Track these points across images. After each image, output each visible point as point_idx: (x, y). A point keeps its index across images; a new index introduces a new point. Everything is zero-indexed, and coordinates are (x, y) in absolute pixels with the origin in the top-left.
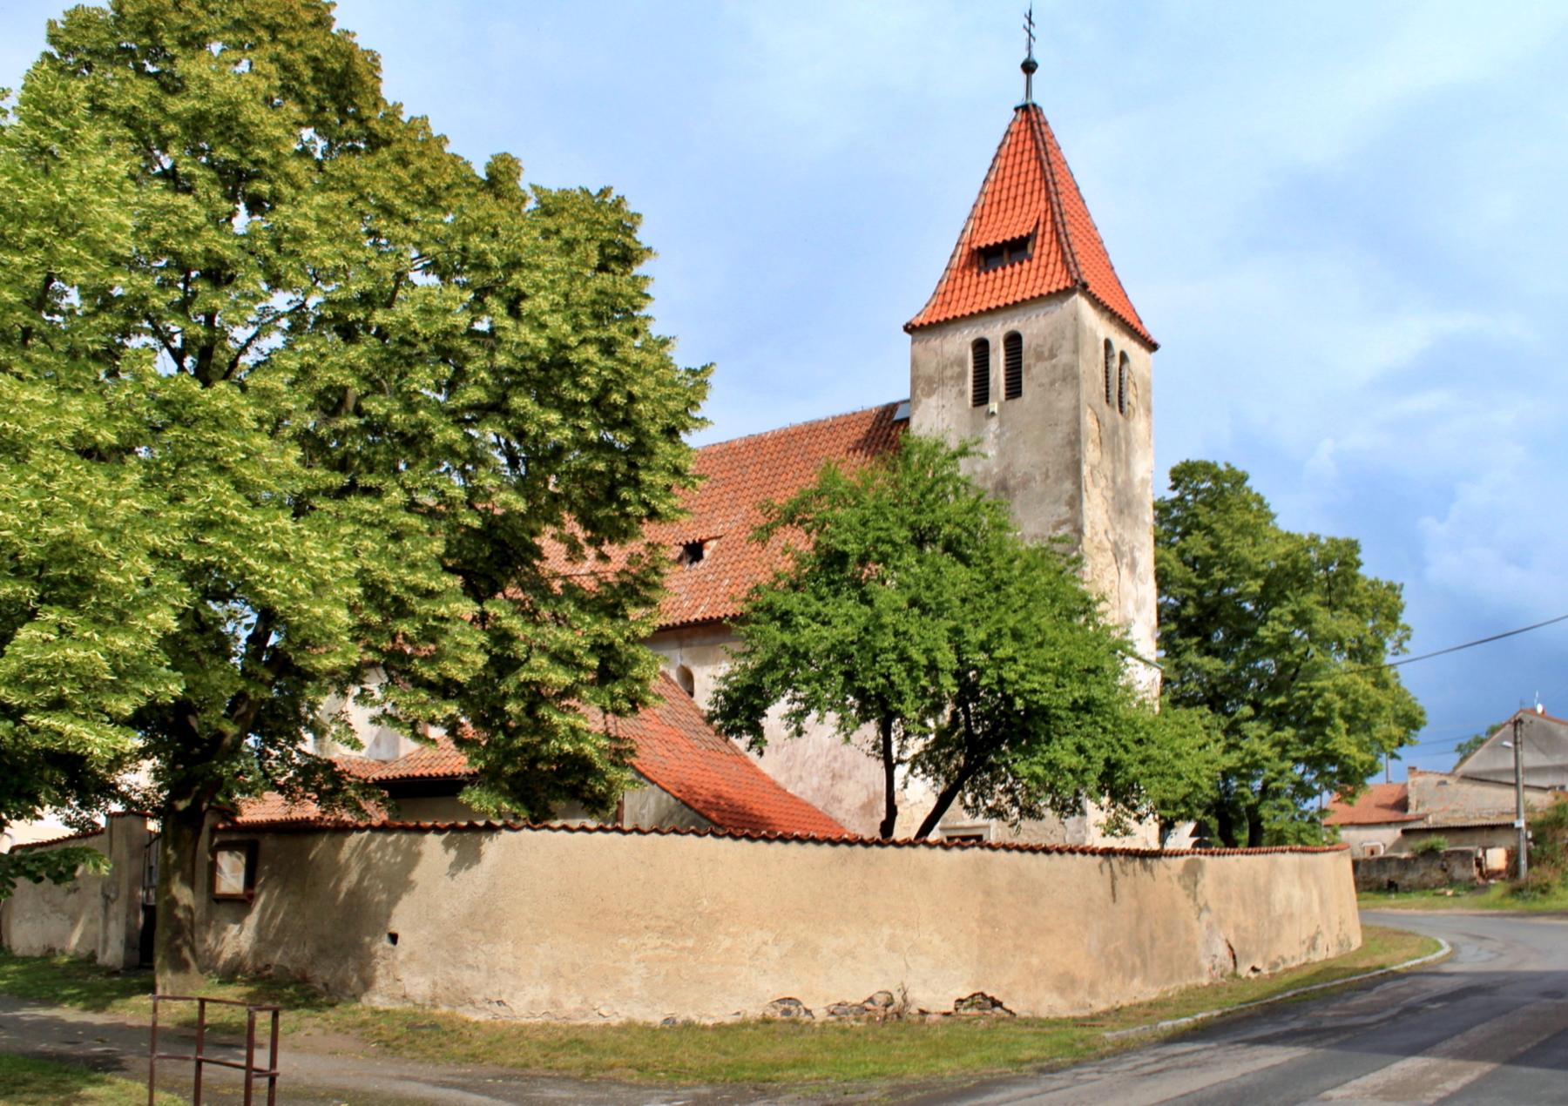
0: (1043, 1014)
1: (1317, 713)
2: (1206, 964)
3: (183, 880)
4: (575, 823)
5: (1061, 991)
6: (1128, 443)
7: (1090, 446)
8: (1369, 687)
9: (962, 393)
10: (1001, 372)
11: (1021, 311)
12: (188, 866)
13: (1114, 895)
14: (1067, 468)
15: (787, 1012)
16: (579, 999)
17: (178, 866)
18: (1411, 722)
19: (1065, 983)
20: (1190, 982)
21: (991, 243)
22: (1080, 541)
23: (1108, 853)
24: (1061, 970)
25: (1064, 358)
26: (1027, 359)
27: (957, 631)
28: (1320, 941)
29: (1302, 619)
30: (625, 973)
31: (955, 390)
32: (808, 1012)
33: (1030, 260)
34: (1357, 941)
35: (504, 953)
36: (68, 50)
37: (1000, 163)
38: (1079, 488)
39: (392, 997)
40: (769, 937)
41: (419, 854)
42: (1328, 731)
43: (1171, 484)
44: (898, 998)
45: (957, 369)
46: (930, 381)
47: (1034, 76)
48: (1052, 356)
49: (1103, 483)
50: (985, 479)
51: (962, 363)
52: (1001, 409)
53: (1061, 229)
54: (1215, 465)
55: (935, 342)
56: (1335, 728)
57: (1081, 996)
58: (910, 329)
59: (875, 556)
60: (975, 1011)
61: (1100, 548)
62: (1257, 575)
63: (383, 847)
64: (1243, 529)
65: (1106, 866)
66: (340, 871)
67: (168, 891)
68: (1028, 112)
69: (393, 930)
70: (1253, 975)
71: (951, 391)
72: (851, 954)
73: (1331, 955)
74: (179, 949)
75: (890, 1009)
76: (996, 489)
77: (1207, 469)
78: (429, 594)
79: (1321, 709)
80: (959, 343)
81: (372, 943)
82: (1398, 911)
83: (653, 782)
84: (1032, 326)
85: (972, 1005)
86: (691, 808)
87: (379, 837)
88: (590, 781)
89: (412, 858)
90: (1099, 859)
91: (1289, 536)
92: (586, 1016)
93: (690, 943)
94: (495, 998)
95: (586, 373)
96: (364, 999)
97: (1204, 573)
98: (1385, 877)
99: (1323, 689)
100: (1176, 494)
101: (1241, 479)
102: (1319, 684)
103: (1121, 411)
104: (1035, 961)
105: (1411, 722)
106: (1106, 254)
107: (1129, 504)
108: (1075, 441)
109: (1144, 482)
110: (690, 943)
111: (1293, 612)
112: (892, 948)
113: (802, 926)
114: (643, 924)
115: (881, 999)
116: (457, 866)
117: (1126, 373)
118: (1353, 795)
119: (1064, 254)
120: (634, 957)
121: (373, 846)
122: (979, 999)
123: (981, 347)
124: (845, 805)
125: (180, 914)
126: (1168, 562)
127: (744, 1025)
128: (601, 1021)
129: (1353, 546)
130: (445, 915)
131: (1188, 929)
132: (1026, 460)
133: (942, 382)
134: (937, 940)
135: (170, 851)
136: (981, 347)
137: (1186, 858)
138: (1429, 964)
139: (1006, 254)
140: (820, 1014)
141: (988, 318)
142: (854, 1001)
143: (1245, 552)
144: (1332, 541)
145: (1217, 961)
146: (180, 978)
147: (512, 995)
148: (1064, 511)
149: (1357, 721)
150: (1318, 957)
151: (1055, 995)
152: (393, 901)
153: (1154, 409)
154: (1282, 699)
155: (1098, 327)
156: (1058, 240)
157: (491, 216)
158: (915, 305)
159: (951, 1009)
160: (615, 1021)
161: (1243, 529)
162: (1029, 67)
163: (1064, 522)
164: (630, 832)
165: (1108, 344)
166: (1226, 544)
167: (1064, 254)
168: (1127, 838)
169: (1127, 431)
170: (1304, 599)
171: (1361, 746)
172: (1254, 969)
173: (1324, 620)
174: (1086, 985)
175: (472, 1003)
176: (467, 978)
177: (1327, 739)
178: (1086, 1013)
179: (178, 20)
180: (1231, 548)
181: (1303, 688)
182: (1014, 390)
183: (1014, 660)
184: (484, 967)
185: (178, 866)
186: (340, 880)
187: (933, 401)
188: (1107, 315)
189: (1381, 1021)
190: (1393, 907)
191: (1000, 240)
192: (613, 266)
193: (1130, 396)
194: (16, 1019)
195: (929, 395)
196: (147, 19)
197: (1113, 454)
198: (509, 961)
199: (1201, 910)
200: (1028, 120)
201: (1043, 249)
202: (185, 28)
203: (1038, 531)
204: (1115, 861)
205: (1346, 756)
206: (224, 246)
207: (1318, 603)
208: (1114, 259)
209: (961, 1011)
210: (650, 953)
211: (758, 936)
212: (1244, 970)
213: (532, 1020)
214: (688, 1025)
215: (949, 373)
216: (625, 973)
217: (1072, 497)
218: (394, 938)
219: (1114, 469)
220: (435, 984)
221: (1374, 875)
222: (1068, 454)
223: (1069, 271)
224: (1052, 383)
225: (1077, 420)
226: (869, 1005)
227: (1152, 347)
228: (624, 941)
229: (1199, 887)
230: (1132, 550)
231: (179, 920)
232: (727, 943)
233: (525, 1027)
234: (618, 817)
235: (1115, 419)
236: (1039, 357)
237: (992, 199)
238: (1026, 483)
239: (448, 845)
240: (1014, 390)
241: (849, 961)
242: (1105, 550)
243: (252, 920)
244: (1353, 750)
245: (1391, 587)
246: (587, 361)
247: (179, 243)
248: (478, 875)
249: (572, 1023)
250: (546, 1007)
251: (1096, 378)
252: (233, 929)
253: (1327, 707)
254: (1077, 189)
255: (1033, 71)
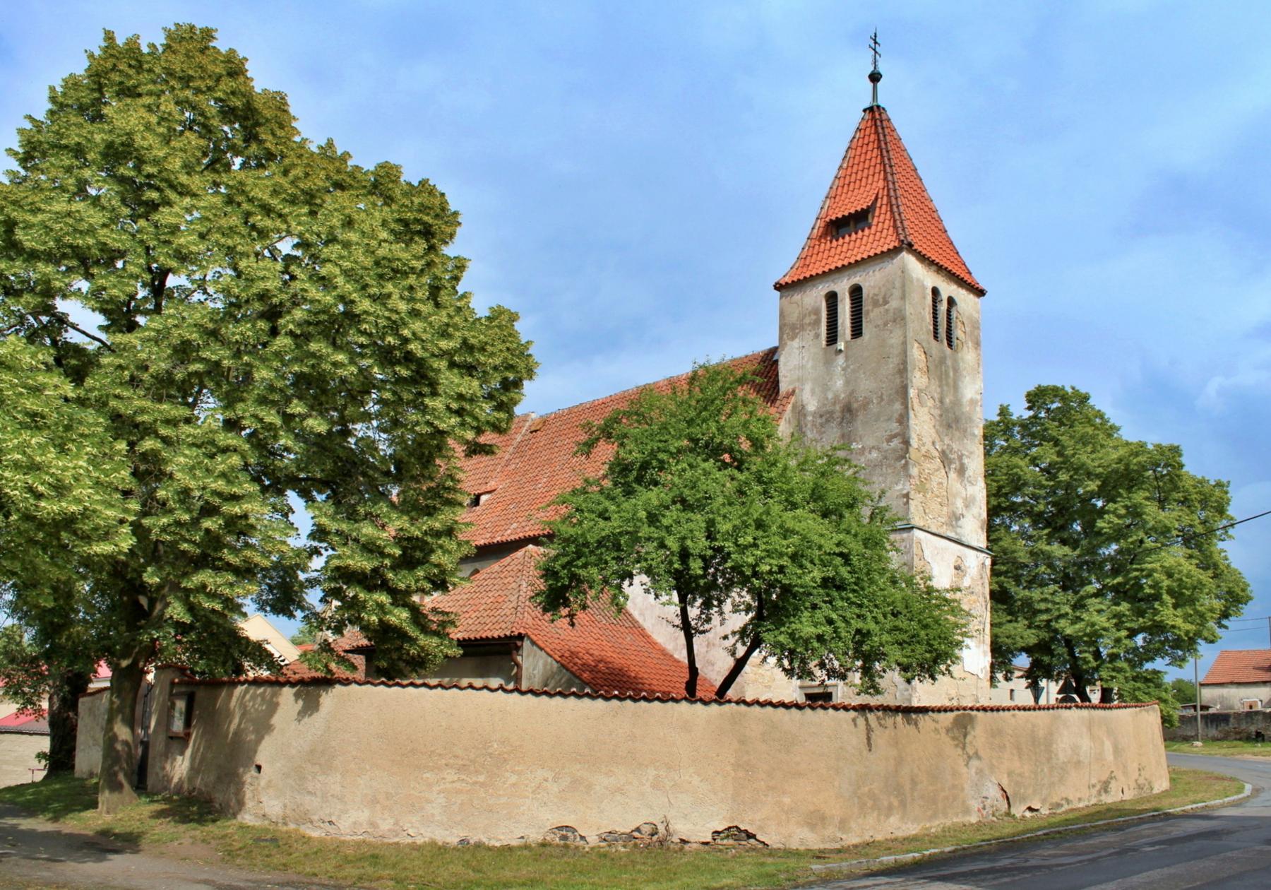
0: (794, 844)
1: (1148, 591)
2: (975, 805)
3: (124, 721)
4: (465, 682)
5: (812, 826)
6: (956, 370)
7: (918, 374)
8: (1193, 568)
9: (817, 336)
10: (847, 319)
11: (862, 268)
12: (127, 710)
13: (869, 744)
14: (897, 392)
15: (564, 838)
16: (392, 821)
17: (120, 710)
18: (1235, 599)
19: (816, 820)
20: (955, 820)
21: (840, 216)
22: (907, 451)
23: (863, 709)
24: (812, 808)
25: (894, 304)
26: (866, 306)
27: (711, 523)
28: (1113, 785)
29: (1135, 512)
30: (429, 801)
31: (812, 333)
32: (582, 838)
33: (870, 228)
34: (1161, 784)
35: (334, 782)
36: (62, 106)
37: (851, 153)
38: (907, 407)
39: (256, 815)
40: (550, 775)
41: (277, 704)
42: (1157, 605)
43: (1027, 405)
44: (661, 829)
45: (813, 317)
46: (793, 327)
47: (879, 84)
48: (886, 302)
49: (930, 403)
50: (834, 404)
51: (817, 312)
52: (846, 347)
53: (894, 202)
54: (1063, 389)
55: (797, 297)
56: (1163, 603)
57: (831, 831)
58: (779, 287)
59: (654, 463)
60: (731, 842)
61: (927, 456)
62: (1089, 475)
63: (253, 698)
64: (1084, 440)
65: (861, 721)
66: (229, 715)
67: (112, 729)
68: (874, 111)
69: (259, 763)
70: (1028, 814)
71: (808, 335)
72: (620, 790)
73: (1128, 796)
74: (115, 774)
75: (655, 838)
76: (843, 412)
77: (1056, 392)
78: (235, 498)
79: (1151, 587)
80: (815, 297)
81: (245, 773)
82: (1260, 758)
83: (542, 649)
84: (870, 280)
85: (727, 837)
86: (567, 670)
87: (252, 690)
88: (406, 646)
89: (273, 707)
90: (852, 714)
91: (1127, 444)
92: (397, 835)
93: (481, 778)
94: (327, 819)
95: (365, 321)
96: (239, 817)
97: (1053, 477)
98: (1253, 729)
99: (1154, 570)
100: (1031, 413)
101: (1084, 399)
102: (1149, 566)
103: (950, 345)
104: (787, 800)
105: (1235, 599)
106: (939, 220)
107: (957, 420)
108: (903, 370)
109: (973, 402)
110: (481, 778)
111: (1126, 507)
112: (656, 786)
113: (578, 766)
114: (444, 762)
115: (647, 829)
116: (303, 713)
117: (954, 314)
118: (1183, 660)
119: (895, 221)
120: (436, 788)
121: (248, 697)
122: (734, 831)
123: (832, 298)
124: (717, 668)
125: (119, 747)
126: (1020, 468)
127: (527, 847)
128: (409, 840)
129: (1175, 450)
130: (294, 752)
131: (955, 774)
132: (866, 386)
133: (802, 328)
134: (696, 780)
135: (114, 699)
136: (832, 298)
137: (956, 713)
138: (1213, 808)
139: (852, 224)
140: (593, 840)
141: (837, 276)
142: (623, 830)
143: (1084, 458)
144: (1159, 447)
145: (988, 802)
146: (116, 796)
147: (339, 817)
148: (895, 427)
149: (1182, 598)
150: (1112, 798)
151: (806, 829)
152: (259, 740)
153: (983, 344)
154: (1120, 579)
155: (926, 278)
156: (891, 211)
157: (344, 208)
158: (782, 268)
159: (709, 839)
160: (420, 841)
161: (1084, 440)
162: (875, 77)
163: (895, 436)
164: (496, 690)
165: (935, 292)
166: (1069, 452)
167: (895, 221)
168: (879, 697)
169: (955, 361)
170: (1135, 495)
171: (1186, 618)
172: (1030, 809)
173: (1152, 512)
174: (836, 821)
175: (312, 822)
176: (310, 803)
177: (1156, 612)
178: (838, 846)
179: (116, 77)
180: (1073, 455)
181: (1137, 570)
182: (857, 331)
183: (755, 545)
184: (319, 794)
185: (120, 710)
186: (230, 723)
187: (796, 343)
188: (934, 268)
189: (1080, 862)
190: (1254, 754)
191: (846, 214)
192: (417, 238)
193: (958, 332)
194: (14, 827)
195: (793, 339)
196: (96, 79)
197: (940, 380)
198: (336, 789)
199: (970, 758)
200: (873, 118)
201: (880, 219)
202: (121, 83)
203: (875, 444)
204: (871, 716)
205: (1173, 627)
206: (115, 240)
207: (1147, 499)
208: (947, 224)
209: (719, 841)
210: (449, 786)
211: (540, 774)
212: (1019, 810)
213: (355, 838)
214: (479, 845)
215: (807, 320)
216: (429, 801)
217: (901, 415)
218: (259, 768)
219: (942, 391)
220: (285, 806)
221: (1244, 726)
222: (898, 381)
223: (898, 235)
224: (885, 324)
225: (905, 353)
226: (636, 834)
227: (980, 293)
228: (428, 775)
229: (969, 738)
230: (960, 457)
231: (118, 752)
232: (514, 779)
233: (343, 842)
234: (517, 679)
235: (943, 352)
236: (876, 304)
237: (844, 180)
238: (866, 404)
239: (297, 696)
240: (857, 331)
241: (618, 797)
242: (933, 458)
243: (188, 752)
244: (1179, 622)
245: (1219, 484)
246: (365, 312)
247: (75, 239)
248: (317, 721)
249: (386, 840)
250: (365, 827)
251: (923, 319)
252: (179, 758)
253: (1156, 585)
254: (915, 170)
255: (878, 80)
